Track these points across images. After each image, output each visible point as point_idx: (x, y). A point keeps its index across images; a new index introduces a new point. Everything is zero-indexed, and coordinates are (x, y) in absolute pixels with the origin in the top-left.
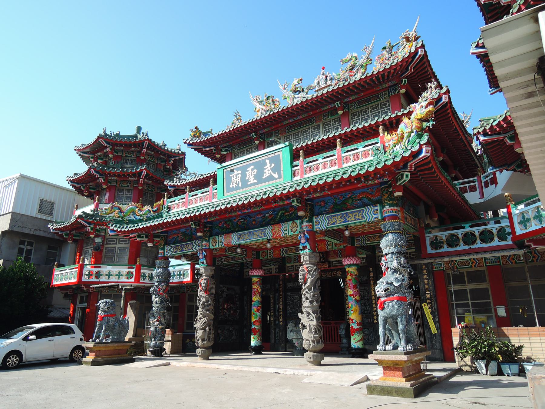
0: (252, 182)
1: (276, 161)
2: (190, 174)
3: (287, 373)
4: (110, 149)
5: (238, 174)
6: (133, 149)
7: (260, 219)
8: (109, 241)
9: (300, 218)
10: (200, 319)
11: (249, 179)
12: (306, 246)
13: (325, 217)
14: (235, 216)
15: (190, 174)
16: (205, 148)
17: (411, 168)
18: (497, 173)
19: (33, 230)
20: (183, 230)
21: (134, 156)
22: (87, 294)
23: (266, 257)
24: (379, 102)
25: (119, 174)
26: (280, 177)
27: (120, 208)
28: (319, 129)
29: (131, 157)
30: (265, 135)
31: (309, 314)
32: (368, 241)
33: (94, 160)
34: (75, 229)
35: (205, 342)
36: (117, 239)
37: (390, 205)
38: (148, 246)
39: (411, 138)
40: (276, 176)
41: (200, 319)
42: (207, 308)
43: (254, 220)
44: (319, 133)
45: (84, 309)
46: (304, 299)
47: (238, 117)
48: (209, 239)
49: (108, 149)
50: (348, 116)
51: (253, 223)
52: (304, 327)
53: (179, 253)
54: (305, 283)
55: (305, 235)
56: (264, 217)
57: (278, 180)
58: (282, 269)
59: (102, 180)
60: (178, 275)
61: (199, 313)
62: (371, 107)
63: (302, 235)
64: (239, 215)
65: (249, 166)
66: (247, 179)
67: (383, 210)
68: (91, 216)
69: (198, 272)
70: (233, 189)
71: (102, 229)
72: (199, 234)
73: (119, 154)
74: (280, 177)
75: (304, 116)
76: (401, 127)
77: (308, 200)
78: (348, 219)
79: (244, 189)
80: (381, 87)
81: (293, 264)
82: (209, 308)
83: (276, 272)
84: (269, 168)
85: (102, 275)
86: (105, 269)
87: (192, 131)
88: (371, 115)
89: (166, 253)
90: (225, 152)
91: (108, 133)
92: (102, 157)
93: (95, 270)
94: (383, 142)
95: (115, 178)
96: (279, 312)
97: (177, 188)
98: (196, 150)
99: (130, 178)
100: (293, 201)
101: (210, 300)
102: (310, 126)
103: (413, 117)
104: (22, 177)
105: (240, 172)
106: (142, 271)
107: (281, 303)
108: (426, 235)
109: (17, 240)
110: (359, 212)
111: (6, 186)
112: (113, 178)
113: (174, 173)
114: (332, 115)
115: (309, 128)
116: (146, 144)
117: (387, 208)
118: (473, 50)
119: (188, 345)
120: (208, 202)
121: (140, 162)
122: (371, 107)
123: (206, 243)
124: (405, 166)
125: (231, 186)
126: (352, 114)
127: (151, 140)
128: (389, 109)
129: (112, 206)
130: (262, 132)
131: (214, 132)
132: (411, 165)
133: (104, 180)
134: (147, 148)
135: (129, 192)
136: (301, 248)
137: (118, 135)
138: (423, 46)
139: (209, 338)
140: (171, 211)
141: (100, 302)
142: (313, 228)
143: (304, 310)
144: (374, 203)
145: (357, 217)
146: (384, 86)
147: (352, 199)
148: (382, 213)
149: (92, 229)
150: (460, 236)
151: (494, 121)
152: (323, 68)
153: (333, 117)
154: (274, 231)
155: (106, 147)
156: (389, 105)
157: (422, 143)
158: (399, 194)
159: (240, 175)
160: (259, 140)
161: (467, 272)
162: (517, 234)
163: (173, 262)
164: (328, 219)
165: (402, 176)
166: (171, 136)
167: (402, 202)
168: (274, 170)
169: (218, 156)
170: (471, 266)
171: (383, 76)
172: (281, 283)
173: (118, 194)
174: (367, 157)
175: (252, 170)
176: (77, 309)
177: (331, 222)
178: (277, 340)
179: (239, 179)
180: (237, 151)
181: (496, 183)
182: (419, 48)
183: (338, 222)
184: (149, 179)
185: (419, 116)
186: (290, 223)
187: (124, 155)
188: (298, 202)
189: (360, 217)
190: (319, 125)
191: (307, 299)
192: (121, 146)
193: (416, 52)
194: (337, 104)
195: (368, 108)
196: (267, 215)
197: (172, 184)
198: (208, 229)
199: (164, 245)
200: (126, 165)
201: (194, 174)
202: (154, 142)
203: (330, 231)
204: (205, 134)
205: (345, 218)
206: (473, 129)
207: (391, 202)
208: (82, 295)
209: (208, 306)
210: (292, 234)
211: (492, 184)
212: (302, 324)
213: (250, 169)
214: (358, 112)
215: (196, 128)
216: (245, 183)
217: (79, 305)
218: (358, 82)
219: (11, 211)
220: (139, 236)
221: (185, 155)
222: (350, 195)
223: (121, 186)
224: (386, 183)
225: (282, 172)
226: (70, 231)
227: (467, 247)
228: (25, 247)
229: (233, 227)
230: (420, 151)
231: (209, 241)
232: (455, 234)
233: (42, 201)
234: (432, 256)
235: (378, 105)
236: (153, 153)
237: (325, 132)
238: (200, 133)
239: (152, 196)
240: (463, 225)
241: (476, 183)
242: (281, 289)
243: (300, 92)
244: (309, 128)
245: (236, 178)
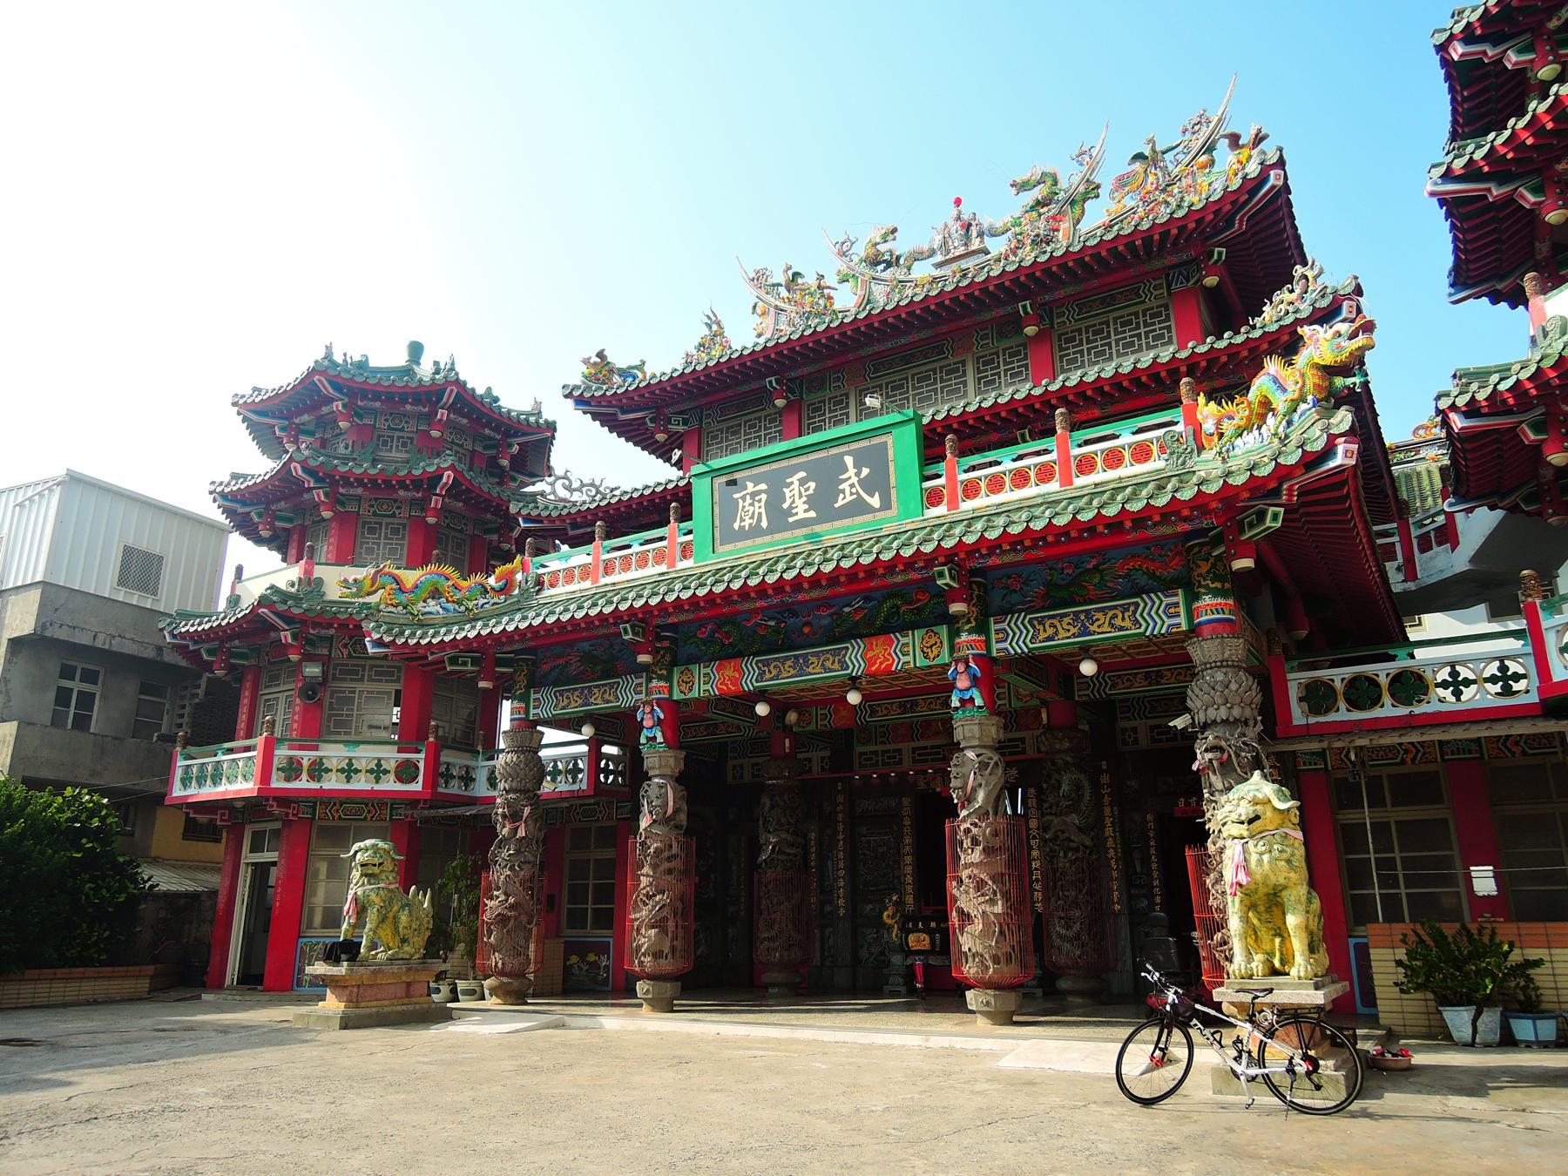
0: (801, 515)
1: (876, 461)
2: (583, 486)
3: (930, 1044)
4: (344, 406)
5: (759, 492)
6: (408, 407)
7: (825, 622)
8: (341, 672)
9: (952, 622)
10: (649, 897)
11: (791, 508)
12: (972, 700)
13: (1024, 618)
14: (749, 611)
15: (583, 486)
16: (624, 412)
17: (1290, 495)
18: (1459, 517)
19: (101, 637)
20: (586, 646)
21: (411, 427)
22: (277, 825)
23: (812, 727)
24: (1140, 308)
25: (373, 480)
26: (886, 505)
27: (397, 580)
28: (964, 374)
29: (402, 430)
30: (801, 384)
31: (980, 884)
32: (1113, 686)
33: (289, 436)
34: (239, 636)
35: (662, 961)
36: (363, 667)
37: (1216, 593)
38: (449, 691)
39: (1296, 417)
40: (875, 501)
41: (649, 897)
42: (666, 865)
43: (807, 624)
44: (965, 384)
45: (261, 871)
46: (967, 843)
47: (715, 327)
48: (670, 673)
49: (338, 406)
50: (1055, 343)
51: (806, 630)
52: (965, 917)
53: (575, 708)
54: (969, 799)
55: (968, 666)
56: (839, 614)
57: (880, 515)
58: (467, 772)
59: (320, 495)
60: (568, 771)
61: (644, 881)
62: (1115, 319)
63: (961, 667)
64: (762, 609)
65: (793, 471)
66: (785, 506)
67: (1196, 605)
68: (296, 598)
69: (447, 769)
70: (743, 535)
71: (321, 638)
72: (643, 658)
73: (366, 421)
74: (886, 505)
75: (922, 335)
76: (1261, 385)
77: (973, 572)
78: (1093, 628)
79: (777, 536)
80: (1148, 267)
81: (873, 748)
82: (672, 865)
83: (823, 769)
84: (854, 480)
85: (328, 770)
86: (333, 753)
87: (586, 361)
88: (1117, 342)
89: (532, 711)
90: (681, 428)
91: (338, 358)
92: (311, 428)
93: (306, 757)
94: (1191, 419)
95: (359, 491)
96: (836, 880)
97: (546, 524)
98: (595, 417)
99: (402, 493)
100: (941, 575)
101: (675, 845)
102: (937, 365)
103: (1301, 359)
104: (75, 482)
105: (763, 486)
106: (443, 759)
107: (841, 855)
108: (1290, 676)
109: (54, 667)
110: (1125, 609)
111: (21, 505)
112: (352, 491)
113: (514, 479)
114: (1002, 335)
115: (934, 371)
116: (448, 397)
117: (1207, 600)
118: (1436, 184)
119: (576, 971)
120: (663, 568)
121: (436, 449)
122: (1115, 319)
123: (662, 684)
124: (1276, 492)
125: (736, 526)
126: (1060, 336)
127: (465, 383)
128: (1169, 329)
129: (376, 573)
130: (799, 372)
131: (649, 370)
132: (1290, 489)
133: (326, 494)
134: (451, 409)
135: (395, 531)
136: (955, 703)
137: (362, 365)
138: (1281, 163)
139: (673, 949)
140: (547, 592)
141: (356, 847)
142: (988, 648)
143: (964, 874)
144: (1168, 587)
145: (1118, 622)
146: (1158, 264)
147: (1101, 572)
148: (1190, 615)
149: (294, 637)
150: (1383, 681)
151: (1502, 379)
152: (958, 202)
153: (1006, 343)
154: (870, 654)
155: (331, 400)
156: (1168, 316)
157: (1334, 431)
158: (1246, 563)
159: (764, 497)
160: (786, 398)
161: (1389, 776)
162: (1556, 679)
163: (551, 735)
164: (1033, 627)
165: (1261, 516)
166: (523, 374)
167: (1242, 588)
168: (868, 485)
169: (660, 437)
170: (1403, 761)
171: (1165, 235)
172: (840, 799)
173: (363, 536)
174: (1146, 460)
175: (802, 482)
176: (242, 867)
177: (1043, 636)
178: (875, 958)
179: (760, 508)
180: (715, 426)
181: (1455, 544)
182: (1273, 166)
183: (1062, 634)
184: (457, 497)
185: (1328, 359)
186: (919, 633)
187: (381, 424)
188: (952, 578)
189: (1127, 623)
190: (963, 363)
191: (975, 842)
192: (376, 397)
193: (1262, 178)
194: (1024, 307)
195: (1107, 323)
196: (847, 610)
197: (534, 513)
198: (666, 644)
199: (528, 688)
200: (400, 459)
201: (592, 485)
202: (473, 390)
203: (1034, 657)
204: (624, 373)
205: (1083, 625)
206: (1438, 398)
207: (1218, 585)
208: (259, 827)
209: (669, 859)
210: (926, 663)
211: (1440, 544)
212: (961, 912)
213: (795, 479)
214: (1079, 331)
215: (601, 355)
216: (779, 517)
217: (248, 857)
218: (1198, 216)
219: (39, 578)
220: (454, 661)
221: (555, 430)
222: (1094, 562)
223: (374, 514)
224: (1203, 532)
225: (893, 493)
226: (222, 642)
227: (1402, 711)
228: (76, 686)
229: (742, 640)
230: (1328, 451)
231: (668, 678)
232: (1370, 674)
233: (128, 552)
234: (1307, 732)
235: (1136, 315)
236: (465, 421)
237: (986, 383)
238: (611, 371)
239: (459, 546)
240: (1392, 652)
241: (1396, 539)
242: (840, 817)
243: (889, 264)
244: (934, 371)
245: (751, 506)
